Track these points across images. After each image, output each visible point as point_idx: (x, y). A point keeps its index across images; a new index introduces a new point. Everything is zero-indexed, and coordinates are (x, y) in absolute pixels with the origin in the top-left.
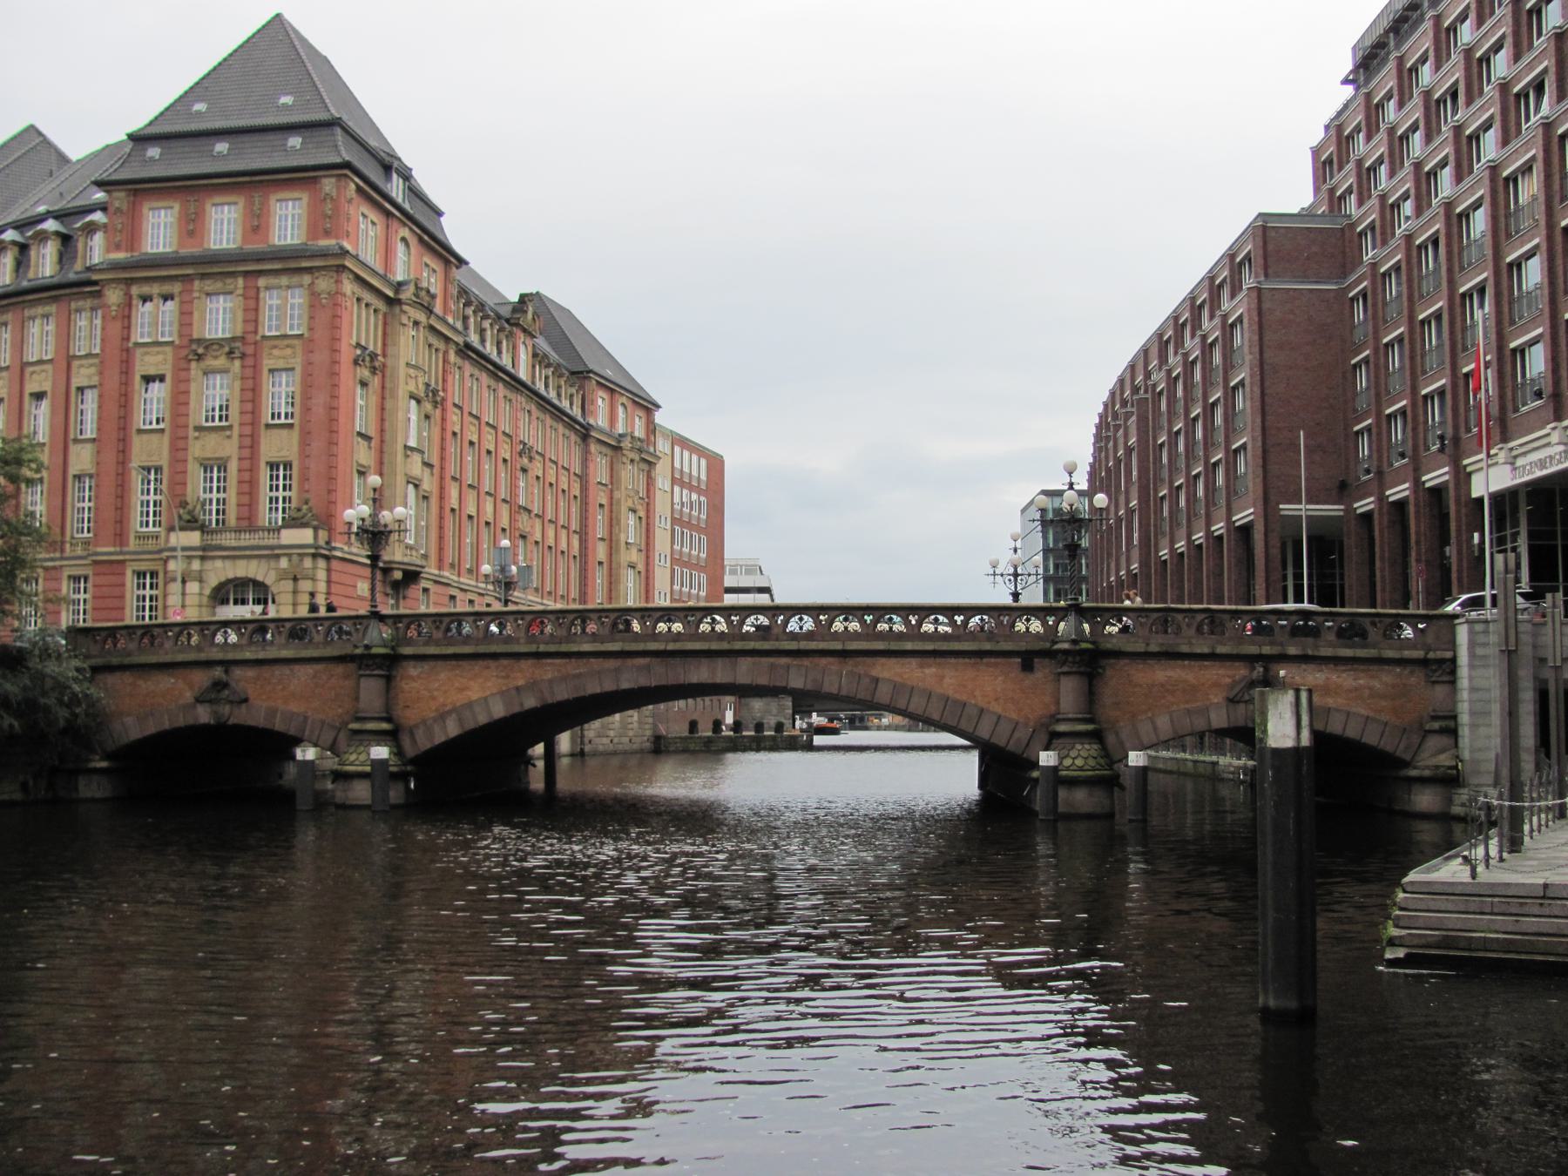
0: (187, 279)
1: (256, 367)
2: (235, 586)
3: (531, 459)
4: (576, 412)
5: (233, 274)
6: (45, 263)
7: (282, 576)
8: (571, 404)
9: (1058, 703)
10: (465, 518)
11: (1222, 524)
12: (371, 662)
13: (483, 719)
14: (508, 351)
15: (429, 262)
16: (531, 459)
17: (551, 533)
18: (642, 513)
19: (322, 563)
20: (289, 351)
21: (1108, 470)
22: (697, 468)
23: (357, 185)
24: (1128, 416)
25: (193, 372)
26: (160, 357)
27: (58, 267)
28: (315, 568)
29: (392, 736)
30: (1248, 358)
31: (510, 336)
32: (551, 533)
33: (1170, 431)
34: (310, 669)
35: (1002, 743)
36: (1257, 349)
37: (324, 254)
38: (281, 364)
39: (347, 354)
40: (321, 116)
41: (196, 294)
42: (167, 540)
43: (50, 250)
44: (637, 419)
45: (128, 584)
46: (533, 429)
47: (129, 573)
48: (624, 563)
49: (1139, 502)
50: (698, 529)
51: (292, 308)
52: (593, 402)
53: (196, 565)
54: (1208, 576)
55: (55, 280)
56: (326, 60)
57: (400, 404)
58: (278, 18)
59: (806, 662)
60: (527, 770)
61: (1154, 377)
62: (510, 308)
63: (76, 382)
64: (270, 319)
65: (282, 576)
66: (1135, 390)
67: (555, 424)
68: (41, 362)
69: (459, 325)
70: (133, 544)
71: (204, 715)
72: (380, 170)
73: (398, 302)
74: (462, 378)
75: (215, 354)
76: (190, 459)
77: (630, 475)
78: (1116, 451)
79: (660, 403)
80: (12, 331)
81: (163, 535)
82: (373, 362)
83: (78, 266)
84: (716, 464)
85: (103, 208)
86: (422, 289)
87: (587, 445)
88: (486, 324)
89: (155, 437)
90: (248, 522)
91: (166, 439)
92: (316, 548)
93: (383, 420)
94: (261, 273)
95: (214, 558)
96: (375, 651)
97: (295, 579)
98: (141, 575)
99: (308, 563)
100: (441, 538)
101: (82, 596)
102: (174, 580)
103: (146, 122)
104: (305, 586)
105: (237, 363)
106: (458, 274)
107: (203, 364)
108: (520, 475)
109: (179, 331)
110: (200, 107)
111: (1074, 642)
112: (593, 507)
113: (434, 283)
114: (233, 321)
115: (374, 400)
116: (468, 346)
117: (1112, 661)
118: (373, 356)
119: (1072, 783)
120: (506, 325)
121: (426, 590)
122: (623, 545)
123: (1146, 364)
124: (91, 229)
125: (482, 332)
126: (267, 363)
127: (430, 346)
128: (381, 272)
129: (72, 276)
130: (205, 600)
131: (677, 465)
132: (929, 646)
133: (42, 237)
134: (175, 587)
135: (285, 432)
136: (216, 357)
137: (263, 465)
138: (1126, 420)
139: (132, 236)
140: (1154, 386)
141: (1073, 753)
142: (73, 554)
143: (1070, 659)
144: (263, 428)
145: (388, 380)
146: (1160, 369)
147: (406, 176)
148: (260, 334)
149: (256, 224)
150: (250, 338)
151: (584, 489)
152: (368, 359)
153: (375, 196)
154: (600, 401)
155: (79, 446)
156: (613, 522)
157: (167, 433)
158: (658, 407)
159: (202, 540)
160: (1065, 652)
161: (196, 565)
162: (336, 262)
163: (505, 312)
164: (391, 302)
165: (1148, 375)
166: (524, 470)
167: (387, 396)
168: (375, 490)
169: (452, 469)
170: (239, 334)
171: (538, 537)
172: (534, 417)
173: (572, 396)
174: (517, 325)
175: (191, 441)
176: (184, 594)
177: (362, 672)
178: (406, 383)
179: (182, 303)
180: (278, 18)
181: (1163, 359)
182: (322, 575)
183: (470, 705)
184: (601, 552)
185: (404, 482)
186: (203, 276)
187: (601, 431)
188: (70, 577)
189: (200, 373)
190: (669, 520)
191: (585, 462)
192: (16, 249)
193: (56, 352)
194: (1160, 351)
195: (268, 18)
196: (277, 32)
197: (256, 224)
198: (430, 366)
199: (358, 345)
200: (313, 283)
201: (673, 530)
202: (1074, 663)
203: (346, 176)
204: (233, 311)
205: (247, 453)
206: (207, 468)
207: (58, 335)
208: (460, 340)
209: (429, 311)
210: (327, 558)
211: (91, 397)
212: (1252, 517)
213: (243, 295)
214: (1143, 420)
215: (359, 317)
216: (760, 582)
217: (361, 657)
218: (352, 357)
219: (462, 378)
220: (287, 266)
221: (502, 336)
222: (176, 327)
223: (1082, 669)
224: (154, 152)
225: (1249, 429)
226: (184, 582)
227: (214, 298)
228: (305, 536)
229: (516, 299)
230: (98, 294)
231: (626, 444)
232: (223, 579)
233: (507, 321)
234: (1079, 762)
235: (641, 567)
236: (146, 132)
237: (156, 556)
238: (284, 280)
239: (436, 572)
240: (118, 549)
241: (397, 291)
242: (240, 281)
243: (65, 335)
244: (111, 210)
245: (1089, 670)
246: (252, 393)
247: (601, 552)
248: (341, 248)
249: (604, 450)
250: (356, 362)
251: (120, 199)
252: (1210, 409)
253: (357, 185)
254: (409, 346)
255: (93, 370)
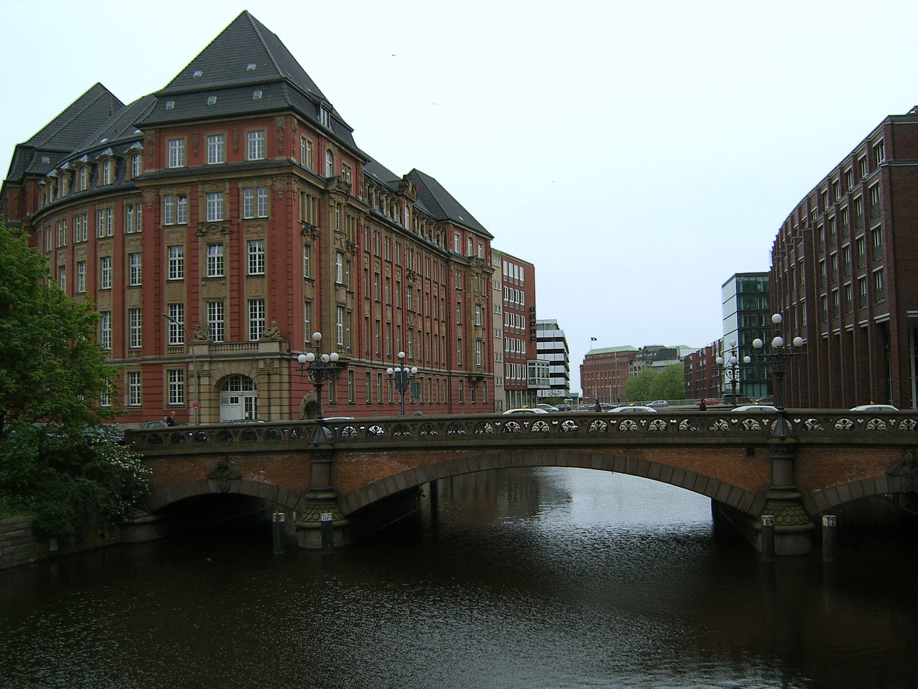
0: (194, 185)
1: (239, 239)
2: (232, 379)
3: (414, 280)
4: (441, 246)
5: (222, 181)
6: (108, 175)
7: (261, 372)
8: (438, 241)
9: (772, 477)
10: (374, 322)
11: (866, 321)
12: (318, 454)
13: (392, 490)
14: (397, 213)
15: (345, 163)
16: (414, 280)
17: (428, 324)
18: (484, 306)
19: (285, 364)
20: (259, 229)
21: (784, 274)
22: (518, 274)
23: (298, 120)
24: (798, 241)
25: (200, 244)
26: (179, 235)
27: (115, 178)
28: (281, 367)
29: (334, 502)
30: (883, 213)
31: (399, 203)
32: (428, 324)
33: (827, 255)
34: (279, 458)
35: (734, 504)
36: (889, 208)
37: (279, 166)
38: (255, 237)
39: (296, 229)
40: (273, 77)
41: (200, 194)
42: (188, 352)
43: (109, 168)
44: (479, 246)
45: (165, 378)
46: (413, 262)
47: (165, 371)
48: (474, 339)
49: (807, 299)
50: (520, 313)
51: (261, 201)
52: (452, 239)
53: (206, 367)
54: (857, 354)
55: (113, 187)
56: (274, 39)
57: (331, 257)
58: (245, 14)
59: (603, 451)
60: (419, 499)
61: (815, 218)
62: (397, 184)
63: (128, 250)
64: (247, 209)
65: (261, 372)
66: (802, 224)
67: (428, 255)
68: (107, 238)
69: (366, 201)
70: (167, 354)
71: (213, 487)
72: (313, 108)
73: (328, 192)
74: (369, 233)
75: (212, 231)
76: (200, 299)
77: (476, 283)
78: (789, 264)
79: (493, 235)
80: (88, 219)
81: (185, 347)
82: (312, 232)
83: (127, 178)
84: (529, 269)
85: (141, 139)
86: (342, 182)
87: (449, 266)
88: (383, 198)
89: (178, 285)
90: (238, 338)
91: (185, 286)
92: (281, 355)
93: (320, 268)
94: (239, 179)
95: (217, 362)
96: (322, 447)
97: (269, 375)
98: (172, 372)
99: (276, 364)
100: (360, 337)
101: (137, 385)
102: (193, 376)
103: (165, 84)
104: (275, 378)
105: (227, 237)
106: (364, 168)
107: (206, 239)
108: (408, 290)
109: (191, 218)
110: (198, 74)
111: (783, 438)
112: (454, 305)
113: (350, 178)
114: (224, 210)
115: (314, 255)
116: (372, 214)
117: (808, 449)
118: (313, 228)
119: (783, 533)
120: (396, 197)
121: (351, 372)
122: (473, 327)
123: (809, 209)
124: (134, 153)
125: (380, 203)
126: (246, 237)
127: (348, 216)
128: (316, 174)
129: (124, 184)
130: (213, 388)
131: (505, 274)
132: (685, 440)
133: (105, 159)
134: (193, 381)
135: (259, 281)
136: (214, 234)
137: (246, 301)
138: (796, 244)
139: (159, 157)
140: (816, 224)
141: (784, 514)
142: (130, 359)
143: (780, 449)
144: (245, 277)
145: (322, 242)
146: (820, 213)
147: (330, 109)
148: (241, 218)
149: (236, 148)
150: (235, 221)
151: (448, 294)
152: (309, 230)
153: (310, 126)
154: (456, 237)
155: (132, 291)
156: (467, 313)
157: (185, 283)
158: (493, 237)
159: (210, 351)
160: (777, 445)
161: (206, 367)
162: (288, 171)
163: (395, 187)
164: (323, 192)
165: (810, 216)
166: (410, 287)
167: (323, 252)
168: (317, 342)
169: (364, 293)
170: (228, 219)
171: (420, 328)
172: (415, 253)
173: (438, 236)
174: (403, 195)
175: (200, 287)
176: (199, 385)
177: (313, 461)
178: (335, 243)
179: (191, 199)
180: (245, 14)
181: (821, 208)
182: (285, 371)
183: (384, 481)
184: (460, 332)
185: (335, 307)
186: (204, 182)
187: (457, 256)
188: (129, 373)
189: (204, 244)
190: (501, 308)
191: (448, 280)
192: (90, 168)
193: (115, 232)
194: (819, 200)
195: (238, 14)
196: (245, 22)
197: (236, 148)
198: (349, 230)
199: (303, 222)
200: (273, 185)
201: (504, 314)
202: (783, 452)
203: (291, 115)
204: (224, 204)
205: (236, 294)
206: (212, 304)
207: (116, 222)
208: (367, 211)
209: (347, 196)
210: (289, 360)
211: (137, 259)
212: (888, 318)
213: (230, 194)
214: (808, 246)
215: (303, 203)
216: (557, 334)
217: (313, 451)
218: (300, 230)
219: (369, 233)
220: (257, 175)
221: (393, 203)
222: (188, 216)
223: (787, 456)
224: (171, 105)
225: (885, 260)
226: (199, 377)
227: (211, 196)
228: (274, 348)
229: (402, 177)
230: (140, 195)
231: (473, 263)
232: (224, 375)
233: (396, 193)
234: (788, 519)
235: (485, 340)
236: (168, 90)
237: (182, 361)
238: (255, 183)
239: (358, 359)
240: (158, 356)
241: (326, 186)
242: (227, 185)
243: (121, 221)
244: (146, 142)
245: (792, 456)
246: (237, 256)
247: (460, 332)
248: (290, 161)
249: (460, 268)
250: (302, 234)
251: (151, 135)
252: (856, 244)
253: (298, 120)
254: (336, 219)
255: (138, 243)
